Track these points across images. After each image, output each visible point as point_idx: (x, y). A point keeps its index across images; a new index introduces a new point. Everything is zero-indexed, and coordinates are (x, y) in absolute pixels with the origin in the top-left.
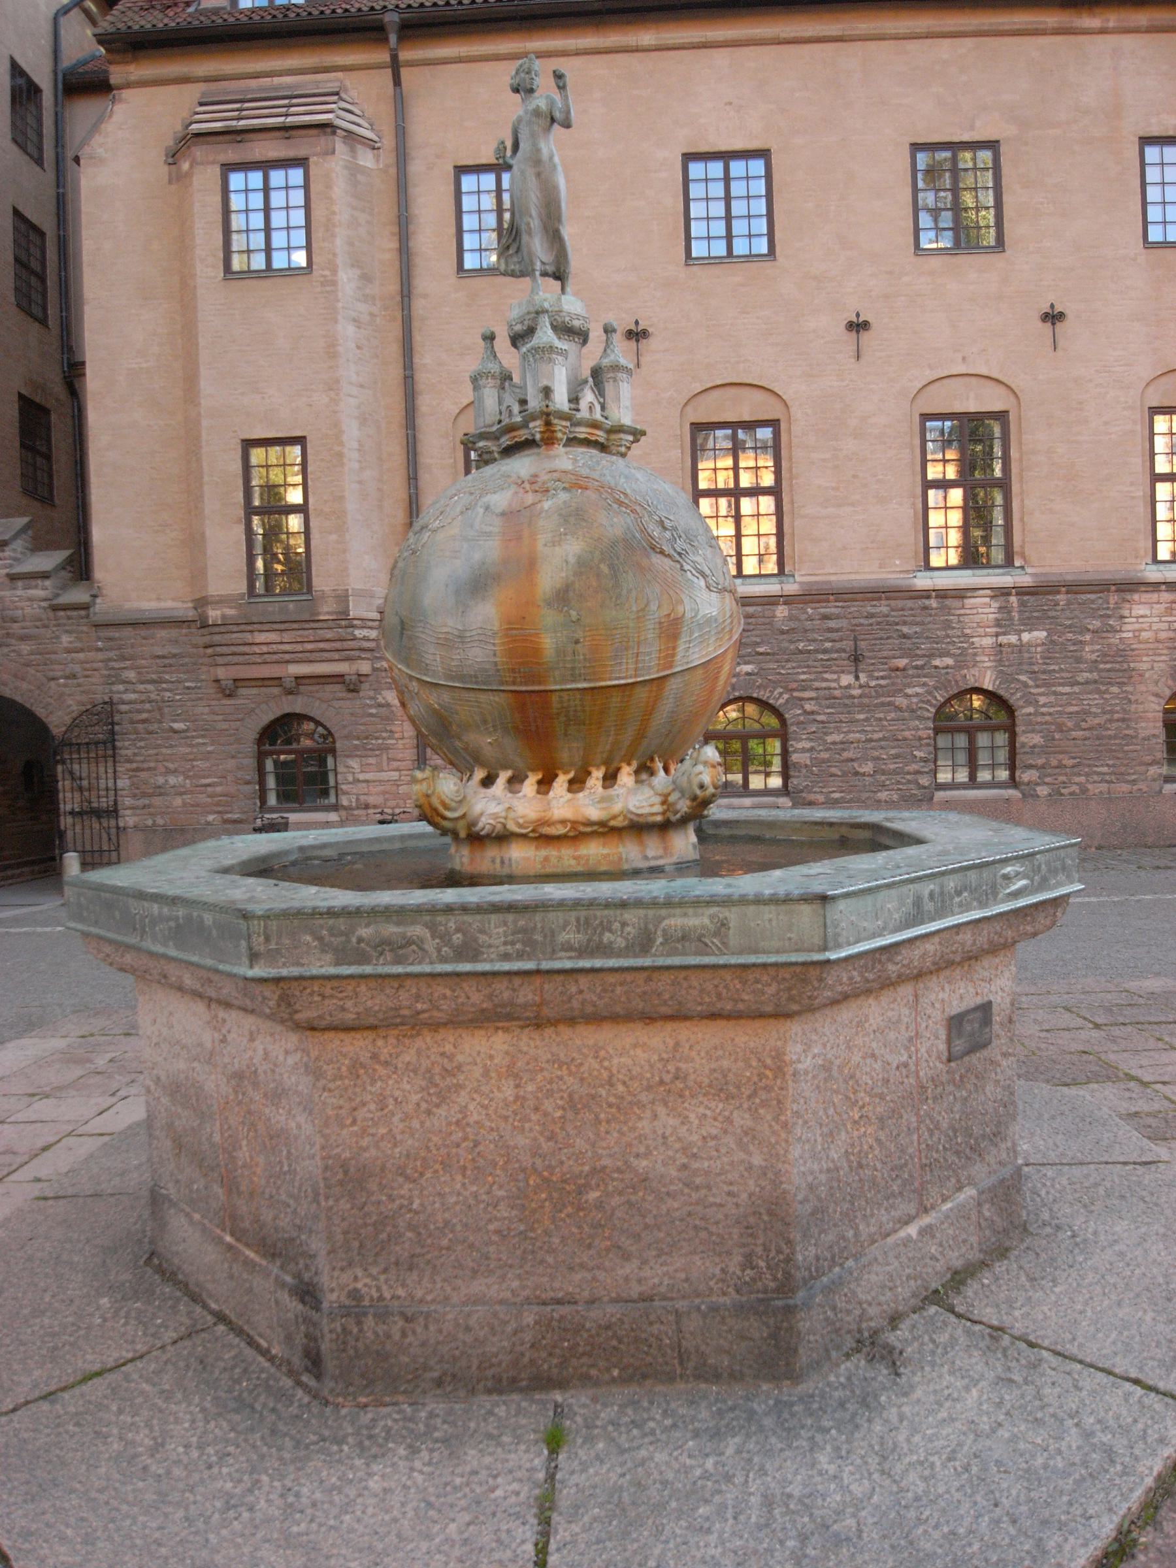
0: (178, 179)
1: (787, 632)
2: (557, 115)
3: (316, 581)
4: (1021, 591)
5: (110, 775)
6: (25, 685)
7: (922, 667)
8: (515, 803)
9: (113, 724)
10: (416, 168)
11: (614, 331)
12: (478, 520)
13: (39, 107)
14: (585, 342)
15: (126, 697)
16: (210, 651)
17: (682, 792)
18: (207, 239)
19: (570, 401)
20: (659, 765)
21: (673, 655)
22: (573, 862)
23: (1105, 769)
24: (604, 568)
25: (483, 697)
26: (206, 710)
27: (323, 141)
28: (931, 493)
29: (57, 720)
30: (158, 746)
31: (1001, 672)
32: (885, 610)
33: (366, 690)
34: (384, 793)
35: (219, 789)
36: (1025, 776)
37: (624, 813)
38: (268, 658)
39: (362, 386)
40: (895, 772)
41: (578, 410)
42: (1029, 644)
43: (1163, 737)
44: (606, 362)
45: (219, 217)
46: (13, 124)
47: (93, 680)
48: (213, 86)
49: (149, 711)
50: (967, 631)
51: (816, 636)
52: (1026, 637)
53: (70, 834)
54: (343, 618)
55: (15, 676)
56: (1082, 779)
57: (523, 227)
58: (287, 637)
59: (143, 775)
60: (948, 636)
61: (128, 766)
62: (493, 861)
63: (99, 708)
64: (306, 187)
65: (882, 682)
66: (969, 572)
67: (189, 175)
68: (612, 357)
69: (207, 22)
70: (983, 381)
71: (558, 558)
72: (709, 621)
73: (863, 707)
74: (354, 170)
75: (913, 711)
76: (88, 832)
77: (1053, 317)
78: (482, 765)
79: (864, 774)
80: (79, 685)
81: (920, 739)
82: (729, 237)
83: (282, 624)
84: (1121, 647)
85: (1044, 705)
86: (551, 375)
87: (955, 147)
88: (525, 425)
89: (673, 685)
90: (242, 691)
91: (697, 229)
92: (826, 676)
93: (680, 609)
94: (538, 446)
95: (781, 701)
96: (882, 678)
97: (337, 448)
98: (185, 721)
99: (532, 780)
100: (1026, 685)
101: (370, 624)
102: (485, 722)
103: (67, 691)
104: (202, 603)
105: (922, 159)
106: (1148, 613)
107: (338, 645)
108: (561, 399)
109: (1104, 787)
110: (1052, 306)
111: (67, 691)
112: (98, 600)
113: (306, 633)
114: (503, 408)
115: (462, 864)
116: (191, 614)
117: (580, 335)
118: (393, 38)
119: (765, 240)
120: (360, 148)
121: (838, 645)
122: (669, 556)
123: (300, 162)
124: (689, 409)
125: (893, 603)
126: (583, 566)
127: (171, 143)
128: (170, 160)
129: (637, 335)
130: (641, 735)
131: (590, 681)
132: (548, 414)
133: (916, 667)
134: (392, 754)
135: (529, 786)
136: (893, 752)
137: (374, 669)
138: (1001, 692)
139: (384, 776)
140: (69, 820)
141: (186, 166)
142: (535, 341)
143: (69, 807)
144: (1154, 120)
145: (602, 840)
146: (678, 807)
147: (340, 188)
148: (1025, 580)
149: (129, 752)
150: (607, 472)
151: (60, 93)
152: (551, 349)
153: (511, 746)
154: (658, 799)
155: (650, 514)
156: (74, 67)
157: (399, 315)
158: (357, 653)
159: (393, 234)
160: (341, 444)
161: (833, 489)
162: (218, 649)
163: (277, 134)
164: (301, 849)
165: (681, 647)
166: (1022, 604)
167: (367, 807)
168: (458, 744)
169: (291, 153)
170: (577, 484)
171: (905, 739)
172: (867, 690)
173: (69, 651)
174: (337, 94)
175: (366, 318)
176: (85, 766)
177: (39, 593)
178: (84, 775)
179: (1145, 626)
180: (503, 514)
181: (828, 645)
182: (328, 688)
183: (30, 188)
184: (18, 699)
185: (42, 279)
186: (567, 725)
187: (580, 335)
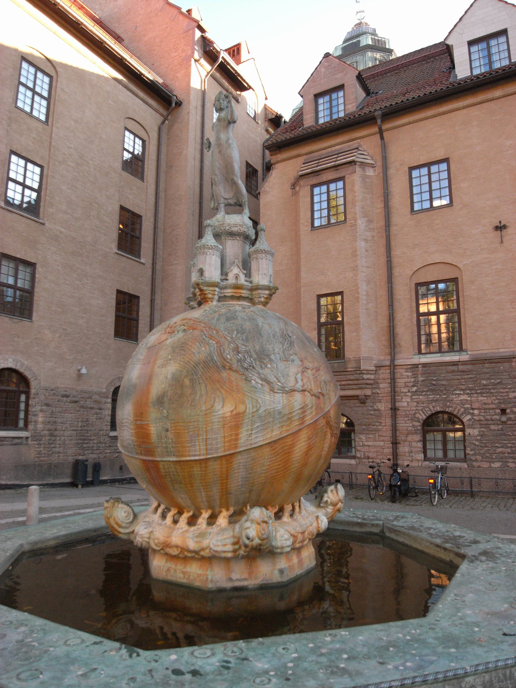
3: (346, 353)
10: (391, 171)
13: (257, 177)
21: (237, 440)
22: (181, 575)
24: (187, 382)
27: (351, 168)
33: (369, 403)
34: (377, 452)
39: (368, 267)
45: (309, 206)
48: (309, 156)
54: (358, 370)
67: (299, 191)
74: (364, 178)
89: (240, 461)
97: (356, 295)
101: (371, 372)
107: (356, 382)
113: (342, 377)
123: (342, 179)
127: (292, 181)
128: (293, 187)
131: (178, 456)
134: (380, 433)
137: (373, 393)
139: (377, 444)
141: (297, 189)
158: (364, 386)
159: (382, 201)
160: (358, 293)
167: (368, 458)
174: (357, 148)
175: (370, 238)
182: (352, 401)
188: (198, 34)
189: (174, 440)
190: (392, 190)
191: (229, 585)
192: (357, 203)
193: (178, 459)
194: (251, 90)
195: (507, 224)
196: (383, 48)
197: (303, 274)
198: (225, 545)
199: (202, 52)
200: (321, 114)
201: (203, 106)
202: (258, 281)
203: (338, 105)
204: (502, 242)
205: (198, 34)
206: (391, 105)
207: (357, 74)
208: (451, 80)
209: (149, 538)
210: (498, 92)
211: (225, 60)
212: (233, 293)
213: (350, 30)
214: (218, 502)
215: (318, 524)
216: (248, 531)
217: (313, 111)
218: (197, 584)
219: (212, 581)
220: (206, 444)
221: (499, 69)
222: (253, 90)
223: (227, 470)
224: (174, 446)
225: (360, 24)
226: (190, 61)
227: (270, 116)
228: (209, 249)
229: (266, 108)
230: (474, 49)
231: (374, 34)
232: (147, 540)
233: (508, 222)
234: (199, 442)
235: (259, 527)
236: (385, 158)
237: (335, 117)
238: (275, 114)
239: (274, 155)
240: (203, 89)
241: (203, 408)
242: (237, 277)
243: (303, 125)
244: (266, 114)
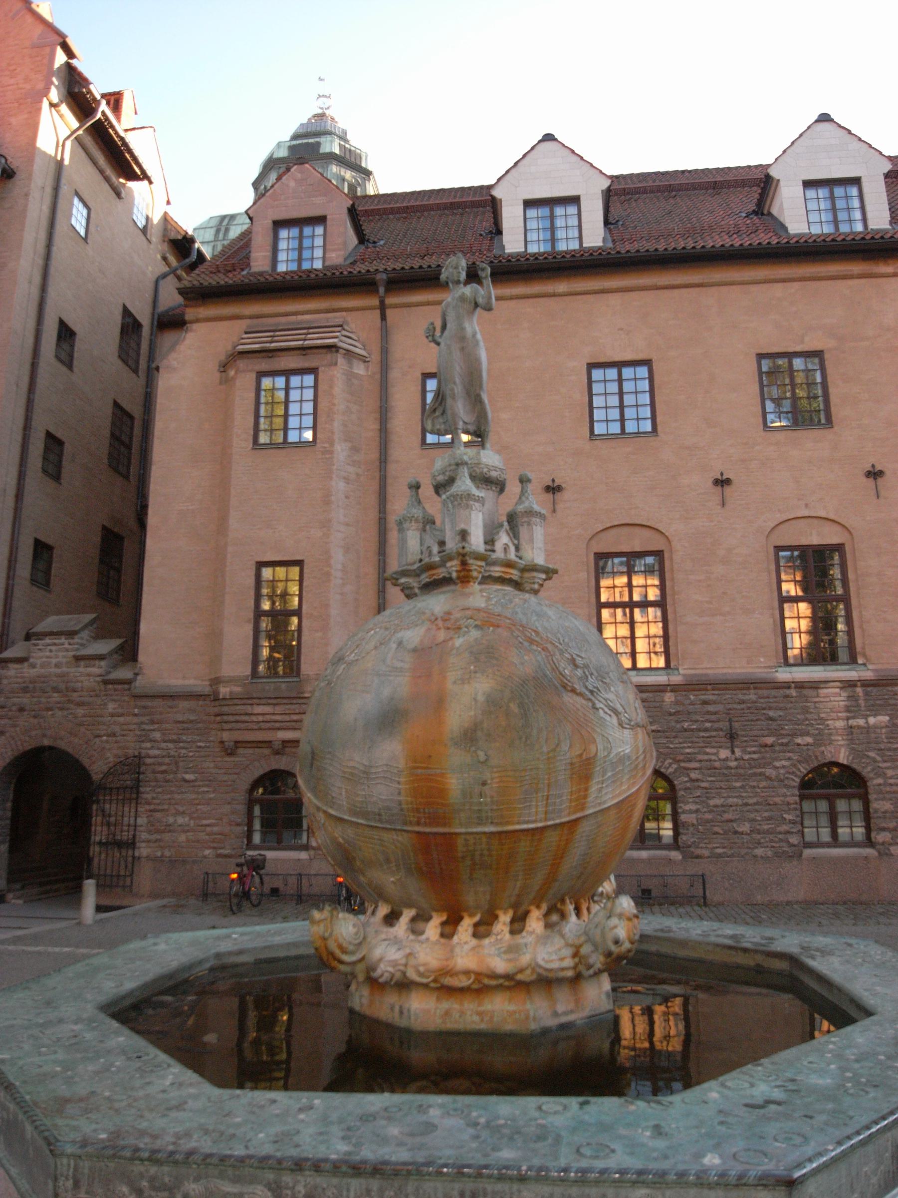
0: (226, 381)
1: (674, 714)
2: (480, 300)
4: (866, 684)
5: (133, 814)
6: (76, 740)
7: (787, 745)
9: (139, 773)
10: (395, 374)
11: (529, 481)
12: (390, 655)
14: (502, 490)
15: (151, 752)
16: (218, 718)
17: (596, 946)
18: (242, 421)
19: (486, 543)
20: (570, 908)
21: (585, 797)
22: (476, 1018)
24: (514, 707)
25: (386, 836)
26: (212, 765)
27: (329, 357)
28: (786, 606)
29: (97, 768)
30: (172, 792)
31: (853, 749)
32: (753, 697)
35: (215, 829)
36: (880, 837)
37: (534, 966)
38: (263, 725)
39: (347, 525)
40: (768, 832)
41: (493, 551)
42: (875, 727)
44: (521, 508)
46: (121, 347)
47: (129, 738)
48: (255, 321)
49: (169, 764)
50: (822, 715)
51: (698, 718)
52: (872, 720)
53: (96, 860)
55: (71, 733)
57: (448, 393)
58: (278, 709)
59: (158, 815)
60: (807, 719)
61: (148, 807)
62: (392, 1009)
63: (130, 760)
64: (316, 387)
65: (755, 756)
67: (233, 379)
68: (527, 504)
69: (255, 281)
70: (822, 521)
71: (467, 696)
72: (621, 759)
73: (739, 776)
74: (350, 376)
75: (782, 781)
76: (110, 859)
78: (387, 900)
79: (742, 833)
80: (116, 742)
81: (789, 804)
82: (622, 420)
83: (276, 699)
85: (891, 778)
86: (468, 520)
87: (790, 356)
88: (443, 563)
89: (585, 828)
90: (241, 751)
91: (598, 415)
92: (708, 750)
93: (593, 749)
94: (455, 584)
95: (670, 770)
96: (754, 752)
97: (326, 569)
98: (193, 773)
99: (437, 920)
100: (875, 761)
102: (388, 861)
103: (107, 746)
104: (216, 681)
105: (766, 365)
108: (477, 541)
110: (873, 466)
111: (107, 746)
112: (139, 678)
113: (293, 707)
114: (424, 549)
115: (362, 1005)
116: (207, 690)
117: (499, 486)
118: (382, 290)
119: (649, 422)
120: (355, 361)
121: (716, 725)
122: (580, 694)
123: (313, 371)
124: (593, 542)
125: (760, 692)
126: (493, 704)
127: (223, 358)
128: (222, 369)
129: (553, 489)
130: (552, 878)
131: (497, 824)
132: (464, 555)
133: (782, 744)
135: (432, 929)
136: (766, 814)
138: (854, 766)
140: (97, 849)
141: (232, 373)
142: (454, 489)
143: (97, 839)
145: (508, 993)
146: (591, 961)
147: (339, 388)
148: (868, 675)
149: (149, 796)
150: (519, 610)
151: (155, 328)
152: (469, 496)
153: (414, 887)
154: (568, 952)
155: (562, 652)
156: (167, 312)
157: (377, 475)
160: (330, 566)
161: (707, 602)
162: (225, 718)
163: (298, 352)
164: (218, 956)
165: (594, 789)
166: (866, 694)
168: (362, 878)
169: (307, 365)
170: (487, 621)
171: (775, 804)
172: (742, 762)
173: (112, 715)
174: (341, 326)
176: (114, 806)
177: (95, 670)
178: (113, 813)
180: (415, 650)
181: (708, 725)
183: (128, 389)
184: (70, 750)
185: (129, 447)
187: (499, 486)
188: (60, 58)
189: (495, 799)
190: (393, 404)
191: (552, 1022)
192: (336, 416)
193: (500, 829)
194: (146, 182)
195: (563, 486)
196: (356, 164)
197: (234, 522)
198: (562, 959)
199: (66, 93)
200: (282, 256)
201: (56, 189)
202: (533, 559)
203: (313, 247)
204: (554, 511)
205: (60, 58)
206: (403, 268)
207: (349, 206)
208: (496, 252)
209: (406, 965)
210: (561, 286)
211: (107, 119)
212: (503, 572)
213: (305, 121)
214: (531, 896)
215: (797, 902)
216: (616, 931)
217: (269, 248)
218: (509, 1027)
219: (534, 1019)
220: (547, 804)
221: (566, 252)
222: (151, 182)
223: (567, 844)
224: (495, 807)
225: (322, 115)
226: (41, 102)
227: (173, 236)
228: (475, 500)
229: (166, 218)
230: (532, 213)
231: (343, 137)
232: (402, 968)
233: (564, 483)
234: (537, 801)
235: (630, 923)
236: (385, 352)
237: (306, 266)
238: (183, 233)
239: (191, 306)
240: (59, 158)
241: (545, 749)
242: (506, 549)
243: (249, 265)
244: (165, 229)
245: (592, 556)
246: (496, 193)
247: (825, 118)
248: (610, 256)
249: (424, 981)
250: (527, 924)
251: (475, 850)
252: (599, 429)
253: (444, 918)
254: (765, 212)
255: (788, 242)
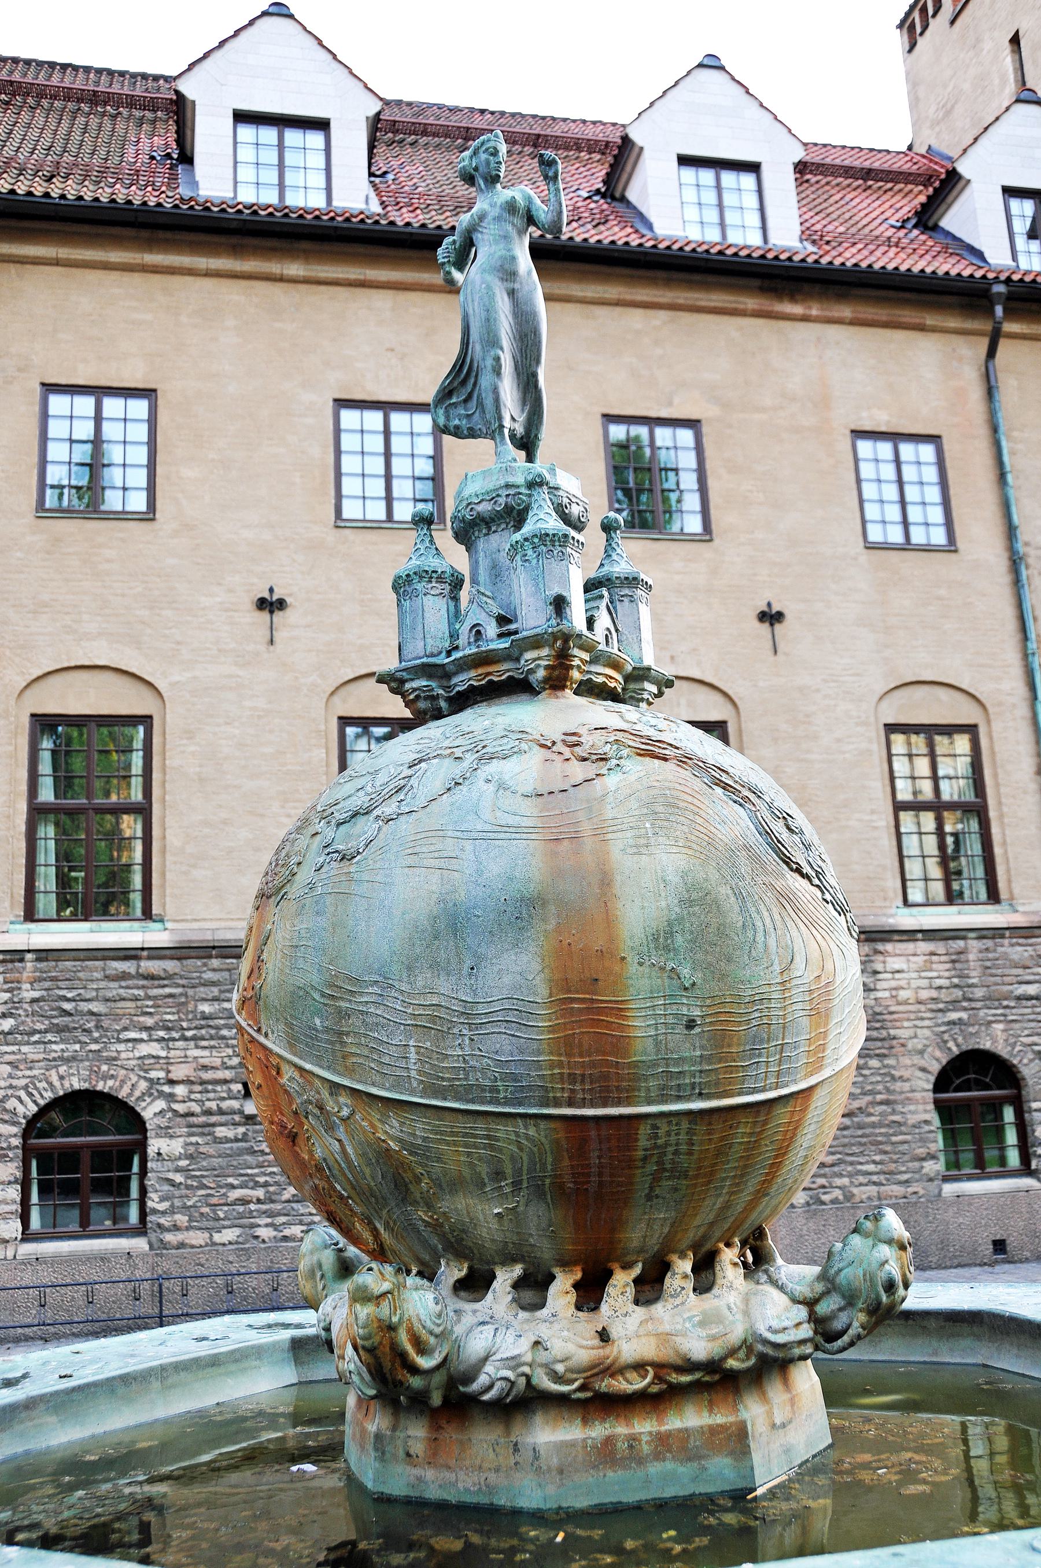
8: (544, 1332)
23: (871, 1167)
25: (503, 1130)
43: (937, 1122)
56: (846, 1181)
66: (86, 925)
77: (771, 617)
84: (878, 1009)
86: (566, 581)
91: (350, 486)
106: (904, 966)
109: (873, 1190)
110: (769, 605)
124: (336, 699)
144: (864, 414)
153: (540, 1225)
179: (903, 983)
186: (656, 1178)
195: (288, 600)
208: (184, 191)
233: (290, 595)
245: (335, 720)
246: (187, 88)
247: (711, 64)
248: (377, 227)
249: (565, 1388)
250: (719, 1274)
251: (667, 1144)
252: (351, 510)
253: (579, 1275)
254: (617, 195)
255: (654, 246)
